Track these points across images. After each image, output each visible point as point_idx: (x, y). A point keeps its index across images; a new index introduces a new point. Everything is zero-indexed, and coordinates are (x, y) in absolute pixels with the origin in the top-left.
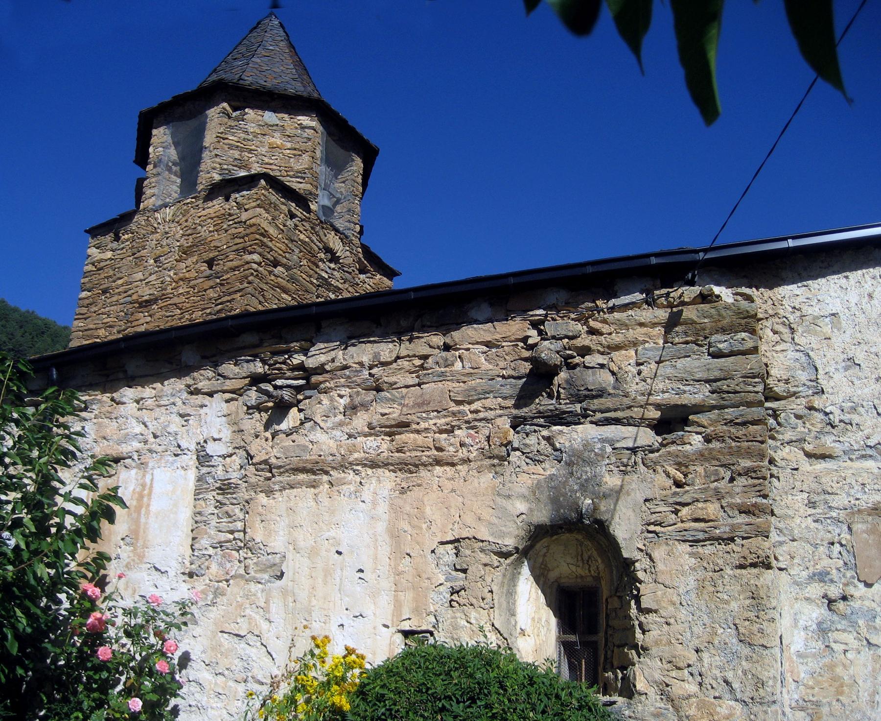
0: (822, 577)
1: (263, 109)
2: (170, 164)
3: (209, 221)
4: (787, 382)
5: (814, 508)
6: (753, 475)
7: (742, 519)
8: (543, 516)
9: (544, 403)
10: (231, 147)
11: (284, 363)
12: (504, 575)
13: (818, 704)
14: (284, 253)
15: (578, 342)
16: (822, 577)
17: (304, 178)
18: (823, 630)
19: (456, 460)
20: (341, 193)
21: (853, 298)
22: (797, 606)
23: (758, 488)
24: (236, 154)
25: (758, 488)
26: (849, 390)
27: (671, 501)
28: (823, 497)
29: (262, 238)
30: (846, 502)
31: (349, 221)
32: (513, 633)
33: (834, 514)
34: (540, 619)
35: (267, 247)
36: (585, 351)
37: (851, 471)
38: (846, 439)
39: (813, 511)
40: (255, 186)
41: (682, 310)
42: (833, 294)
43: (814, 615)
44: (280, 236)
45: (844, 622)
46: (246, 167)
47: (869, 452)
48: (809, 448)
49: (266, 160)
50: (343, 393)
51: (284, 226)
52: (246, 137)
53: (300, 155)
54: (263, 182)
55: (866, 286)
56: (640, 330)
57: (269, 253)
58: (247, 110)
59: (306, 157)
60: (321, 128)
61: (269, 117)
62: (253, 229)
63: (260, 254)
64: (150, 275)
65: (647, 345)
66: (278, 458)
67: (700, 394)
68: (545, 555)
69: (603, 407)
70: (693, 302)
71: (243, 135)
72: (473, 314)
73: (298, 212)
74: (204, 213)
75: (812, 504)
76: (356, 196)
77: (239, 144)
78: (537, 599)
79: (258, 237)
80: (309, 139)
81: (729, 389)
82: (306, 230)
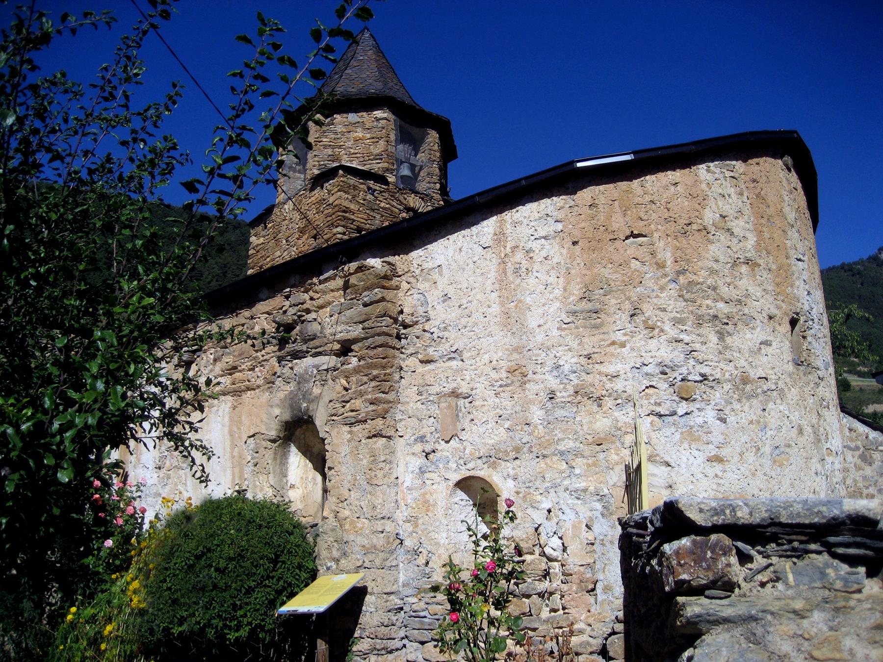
0: (422, 439)
1: (347, 112)
2: (294, 166)
3: (313, 206)
4: (412, 315)
5: (421, 395)
6: (377, 379)
7: (372, 408)
8: (287, 417)
9: (290, 347)
10: (325, 147)
11: (187, 337)
12: (275, 454)
13: (416, 518)
14: (366, 220)
15: (305, 306)
16: (422, 439)
17: (381, 159)
18: (422, 471)
19: (255, 386)
20: (422, 161)
21: (450, 252)
22: (407, 459)
23: (379, 388)
24: (329, 151)
25: (379, 388)
26: (443, 316)
27: (340, 400)
28: (426, 387)
29: (344, 214)
30: (438, 390)
31: (429, 183)
32: (285, 487)
33: (431, 398)
34: (307, 478)
35: (350, 219)
36: (308, 311)
37: (442, 369)
38: (440, 349)
39: (420, 397)
40: (336, 176)
41: (349, 279)
42: (439, 252)
43: (418, 463)
44: (361, 209)
45: (433, 466)
46: (338, 159)
47: (453, 355)
48: (420, 356)
49: (352, 151)
50: (212, 352)
51: (364, 200)
52: (336, 136)
53: (377, 142)
54: (341, 172)
55: (459, 243)
56: (332, 294)
57: (352, 224)
58: (335, 116)
59: (382, 143)
60: (393, 117)
61: (352, 117)
62: (336, 209)
63: (343, 226)
64: (285, 251)
65: (334, 304)
66: (613, 343)
67: (357, 331)
68: (304, 439)
69: (315, 346)
70: (356, 272)
71: (333, 136)
72: (262, 296)
73: (377, 187)
74: (310, 201)
75: (420, 393)
76: (434, 161)
77: (331, 143)
78: (306, 465)
79: (340, 214)
80: (383, 128)
81: (368, 326)
82: (386, 199)
